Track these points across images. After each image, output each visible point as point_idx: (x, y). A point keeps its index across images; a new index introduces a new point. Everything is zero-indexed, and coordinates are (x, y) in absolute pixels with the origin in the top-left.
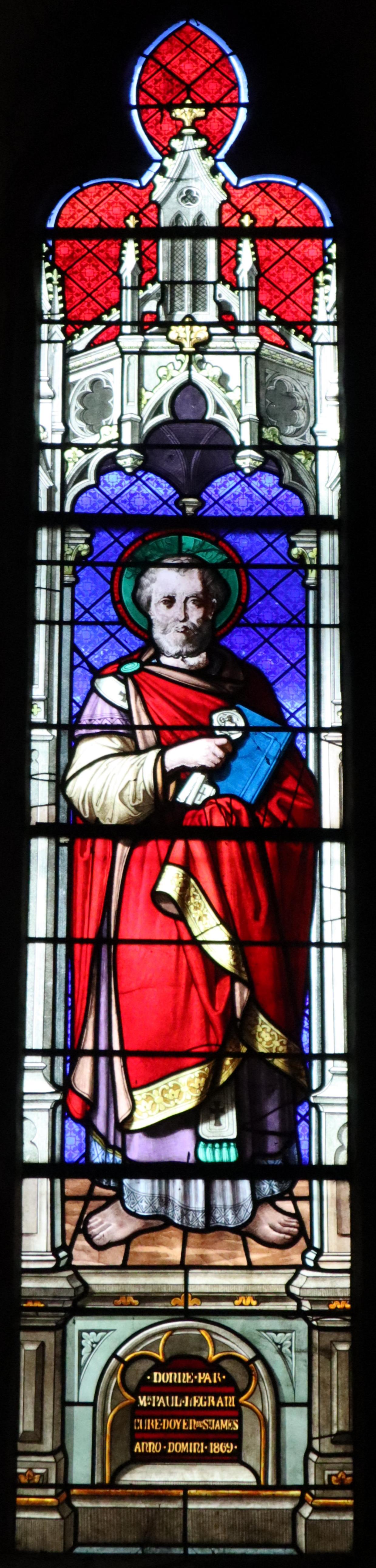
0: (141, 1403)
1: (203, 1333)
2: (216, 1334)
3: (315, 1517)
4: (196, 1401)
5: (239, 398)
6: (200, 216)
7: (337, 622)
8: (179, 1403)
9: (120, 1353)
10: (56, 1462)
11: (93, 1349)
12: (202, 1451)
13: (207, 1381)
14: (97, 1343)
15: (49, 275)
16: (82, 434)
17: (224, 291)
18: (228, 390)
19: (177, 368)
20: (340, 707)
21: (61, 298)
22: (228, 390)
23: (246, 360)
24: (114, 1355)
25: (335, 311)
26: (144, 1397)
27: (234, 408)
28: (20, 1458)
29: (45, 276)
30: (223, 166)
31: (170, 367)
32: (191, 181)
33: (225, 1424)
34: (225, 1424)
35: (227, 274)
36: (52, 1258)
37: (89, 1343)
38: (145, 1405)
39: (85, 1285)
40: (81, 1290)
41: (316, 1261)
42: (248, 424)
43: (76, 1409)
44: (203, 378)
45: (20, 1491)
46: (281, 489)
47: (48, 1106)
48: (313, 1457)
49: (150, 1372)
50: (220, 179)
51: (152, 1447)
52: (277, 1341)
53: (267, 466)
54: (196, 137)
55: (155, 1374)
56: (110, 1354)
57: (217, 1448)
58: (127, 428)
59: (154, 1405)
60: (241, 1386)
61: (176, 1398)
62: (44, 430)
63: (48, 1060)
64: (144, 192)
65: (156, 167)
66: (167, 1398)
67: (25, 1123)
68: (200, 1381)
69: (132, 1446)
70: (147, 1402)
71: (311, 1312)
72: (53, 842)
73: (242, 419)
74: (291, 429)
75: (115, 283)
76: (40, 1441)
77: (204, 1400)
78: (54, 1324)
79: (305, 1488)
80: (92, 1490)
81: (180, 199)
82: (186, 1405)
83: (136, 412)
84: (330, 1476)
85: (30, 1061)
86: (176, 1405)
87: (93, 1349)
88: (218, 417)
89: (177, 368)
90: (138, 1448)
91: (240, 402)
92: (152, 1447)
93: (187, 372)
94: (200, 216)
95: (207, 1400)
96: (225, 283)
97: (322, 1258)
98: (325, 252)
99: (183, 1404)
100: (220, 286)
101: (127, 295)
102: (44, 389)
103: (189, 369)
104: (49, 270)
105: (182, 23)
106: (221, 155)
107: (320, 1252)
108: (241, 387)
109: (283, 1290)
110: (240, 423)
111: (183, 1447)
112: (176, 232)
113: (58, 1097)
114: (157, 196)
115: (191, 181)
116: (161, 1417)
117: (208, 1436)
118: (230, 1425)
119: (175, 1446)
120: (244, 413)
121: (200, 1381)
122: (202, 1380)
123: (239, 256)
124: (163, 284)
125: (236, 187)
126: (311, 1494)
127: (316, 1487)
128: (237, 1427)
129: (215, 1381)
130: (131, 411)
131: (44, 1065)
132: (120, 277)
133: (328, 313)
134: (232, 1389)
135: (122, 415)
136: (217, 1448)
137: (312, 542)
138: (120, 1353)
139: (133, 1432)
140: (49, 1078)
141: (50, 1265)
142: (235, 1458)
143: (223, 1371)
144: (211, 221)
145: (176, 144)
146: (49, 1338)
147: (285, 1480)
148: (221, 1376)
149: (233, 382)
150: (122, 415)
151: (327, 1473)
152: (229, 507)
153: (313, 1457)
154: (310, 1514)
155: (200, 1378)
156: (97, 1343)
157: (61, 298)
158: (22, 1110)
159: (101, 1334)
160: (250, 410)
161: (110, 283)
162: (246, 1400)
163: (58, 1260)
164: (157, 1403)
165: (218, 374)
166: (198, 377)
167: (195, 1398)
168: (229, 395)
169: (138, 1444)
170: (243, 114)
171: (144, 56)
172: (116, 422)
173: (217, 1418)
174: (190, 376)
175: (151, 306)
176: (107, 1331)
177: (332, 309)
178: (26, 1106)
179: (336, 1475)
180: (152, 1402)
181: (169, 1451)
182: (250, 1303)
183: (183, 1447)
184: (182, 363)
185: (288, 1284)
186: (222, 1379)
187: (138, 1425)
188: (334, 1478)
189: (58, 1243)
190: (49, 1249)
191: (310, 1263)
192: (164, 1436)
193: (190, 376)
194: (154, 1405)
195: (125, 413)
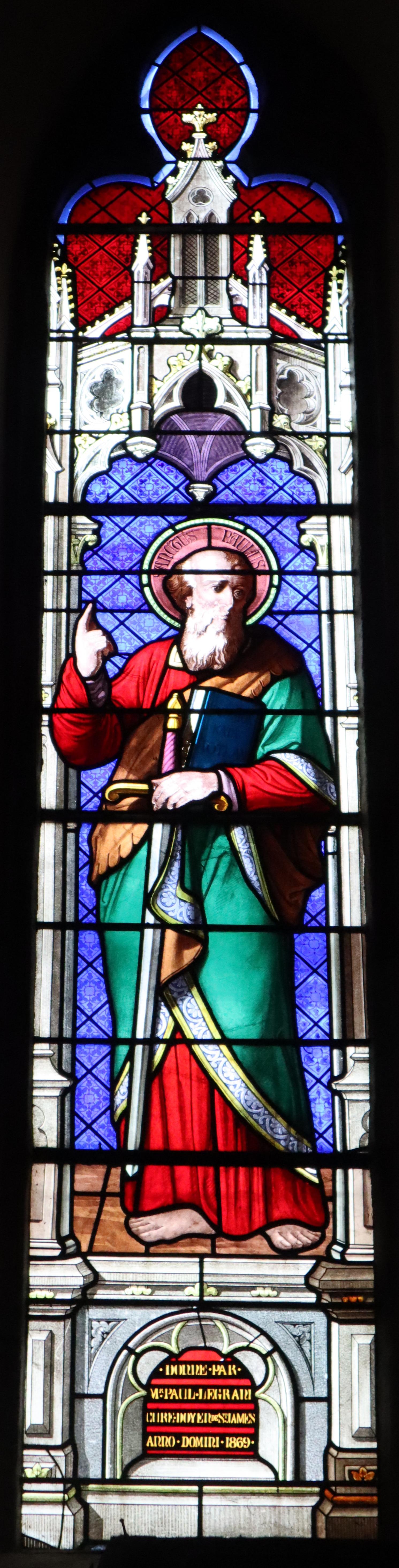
0: (153, 1396)
1: (219, 1324)
2: (233, 1324)
3: (336, 1514)
4: (210, 1394)
5: (249, 387)
6: (211, 215)
7: (351, 608)
8: (192, 1396)
9: (131, 1345)
10: (66, 1456)
11: (104, 1339)
12: (218, 1446)
13: (222, 1373)
14: (108, 1333)
15: (58, 268)
16: (88, 418)
17: (236, 285)
18: (238, 379)
19: (187, 358)
20: (356, 692)
21: (70, 289)
22: (238, 379)
23: (256, 351)
24: (125, 1346)
25: (347, 303)
26: (156, 1390)
27: (244, 397)
28: (26, 1452)
29: (54, 269)
30: (232, 167)
31: (181, 356)
32: (203, 185)
33: (243, 1419)
34: (243, 1419)
35: (239, 270)
36: (57, 1246)
37: (100, 1333)
38: (157, 1398)
39: (96, 1274)
40: (91, 1279)
41: (342, 1254)
42: (258, 411)
43: (87, 1401)
44: (214, 369)
45: (26, 1486)
46: (292, 475)
47: (57, 1093)
48: (333, 1451)
49: (162, 1364)
50: (231, 179)
51: (167, 1441)
52: (295, 1333)
53: (278, 453)
54: (206, 141)
55: (167, 1367)
56: (120, 1346)
57: (233, 1443)
58: (137, 415)
59: (166, 1397)
60: (258, 1380)
61: (190, 1390)
62: (50, 416)
63: (55, 1046)
64: (154, 194)
65: (168, 169)
66: (180, 1390)
67: (35, 1109)
68: (214, 1374)
69: (145, 1440)
70: (159, 1394)
71: (331, 1305)
72: (60, 827)
73: (252, 407)
74: (301, 417)
75: (126, 278)
76: (49, 1433)
77: (218, 1393)
78: (63, 1314)
79: (325, 1485)
80: (101, 1486)
81: (191, 199)
82: (200, 1398)
83: (146, 400)
84: (350, 1471)
85: (40, 1049)
86: (190, 1398)
87: (104, 1339)
88: (229, 406)
89: (187, 358)
90: (150, 1442)
91: (250, 392)
92: (167, 1441)
93: (198, 362)
94: (211, 215)
95: (222, 1393)
96: (236, 278)
97: (349, 1251)
98: (338, 247)
99: (197, 1397)
100: (232, 280)
101: (139, 291)
102: (51, 377)
103: (200, 359)
104: (58, 264)
105: (193, 32)
106: (233, 155)
107: (346, 1246)
108: (251, 376)
109: (302, 1281)
110: (250, 410)
111: (197, 1442)
112: (188, 230)
113: (67, 1084)
114: (169, 195)
115: (203, 185)
116: (174, 1411)
117: (224, 1431)
118: (247, 1419)
119: (189, 1441)
120: (253, 402)
121: (214, 1374)
122: (217, 1373)
123: (251, 252)
124: (175, 279)
125: (249, 187)
126: (331, 1491)
127: (337, 1483)
128: (254, 1419)
129: (230, 1373)
130: (141, 397)
131: (51, 1052)
132: (132, 274)
133: (341, 305)
134: (247, 1382)
135: (131, 402)
136: (233, 1443)
137: (323, 529)
138: (131, 1345)
139: (145, 1425)
140: (56, 1064)
141: (57, 1253)
142: (252, 1454)
143: (239, 1364)
144: (222, 218)
145: (185, 146)
146: (60, 1330)
147: (305, 1474)
148: (236, 1369)
149: (242, 371)
150: (131, 402)
151: (347, 1468)
152: (239, 492)
153: (333, 1451)
154: (331, 1511)
155: (214, 1370)
156: (108, 1333)
157: (70, 289)
158: (32, 1097)
159: (112, 1324)
160: (260, 398)
161: (121, 278)
162: (264, 1393)
163: (64, 1248)
164: (169, 1396)
165: (226, 361)
166: (209, 367)
167: (209, 1390)
168: (239, 384)
169: (150, 1438)
170: (253, 118)
171: (157, 65)
172: (126, 410)
173: (234, 1412)
174: (200, 365)
175: (163, 300)
176: (119, 1321)
177: (344, 302)
178: (36, 1093)
179: (357, 1471)
180: (164, 1395)
181: (183, 1446)
182: (265, 1294)
183: (197, 1442)
184: (192, 353)
185: (307, 1277)
186: (238, 1372)
187: (150, 1418)
188: (354, 1474)
189: (65, 1230)
190: (54, 1237)
191: (336, 1256)
192: (178, 1431)
193: (200, 365)
194: (166, 1397)
195: (134, 401)
